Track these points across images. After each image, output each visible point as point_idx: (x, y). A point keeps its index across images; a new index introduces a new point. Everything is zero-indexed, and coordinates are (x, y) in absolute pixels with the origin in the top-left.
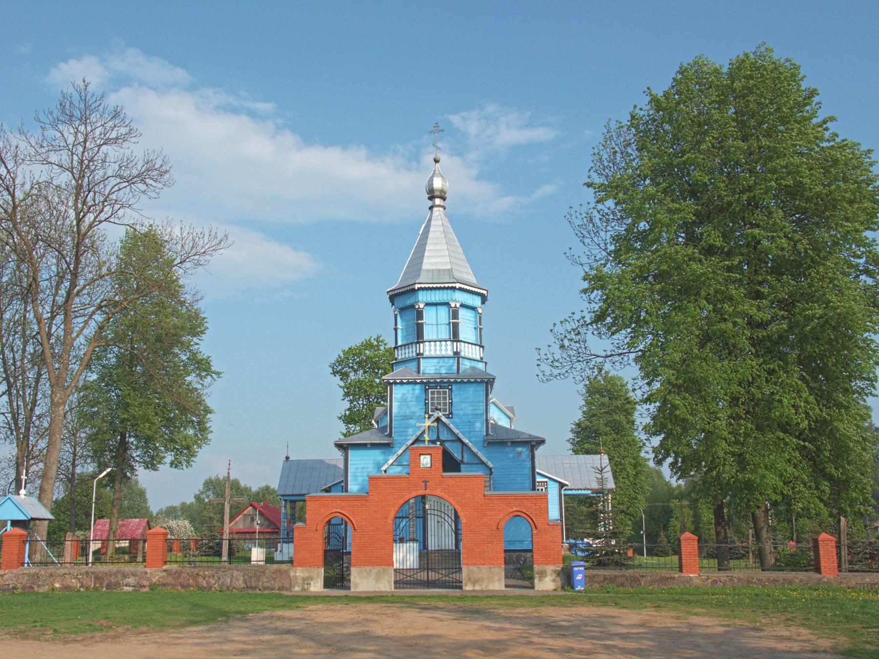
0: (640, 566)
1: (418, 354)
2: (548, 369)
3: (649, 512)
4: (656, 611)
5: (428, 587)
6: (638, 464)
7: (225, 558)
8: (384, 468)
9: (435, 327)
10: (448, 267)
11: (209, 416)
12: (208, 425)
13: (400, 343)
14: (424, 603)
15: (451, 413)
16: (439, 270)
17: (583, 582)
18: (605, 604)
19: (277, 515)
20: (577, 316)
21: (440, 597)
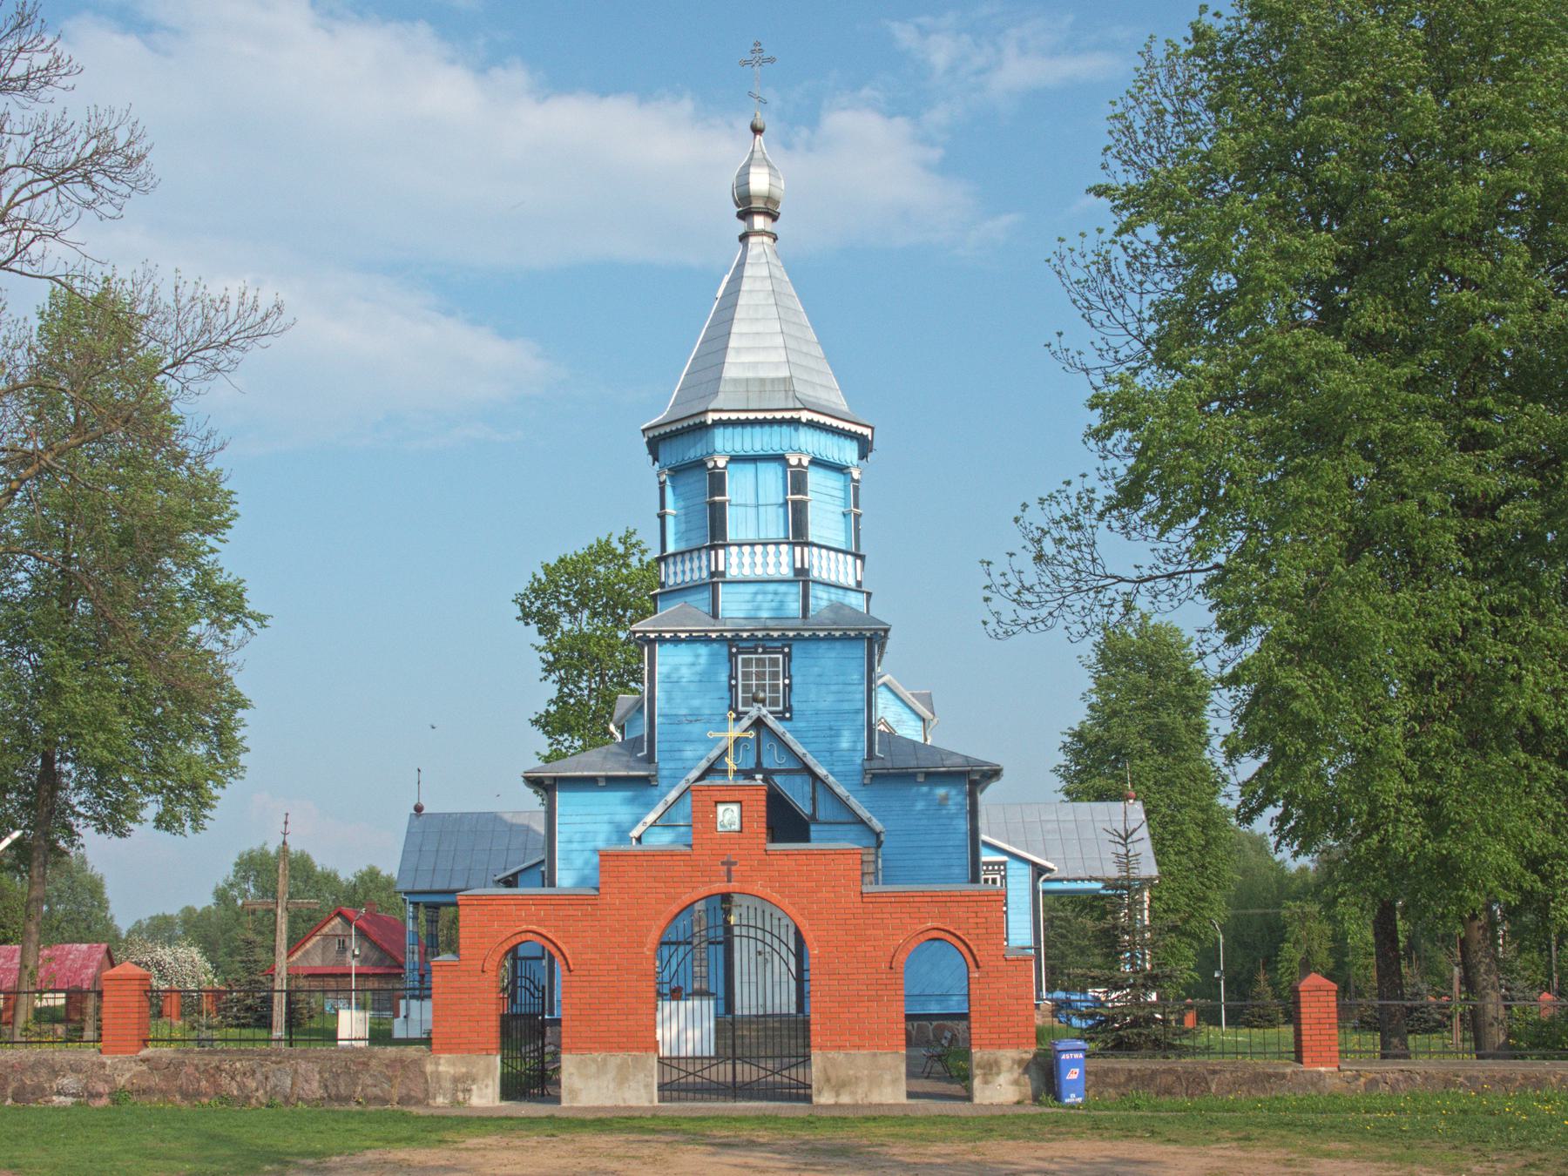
0: (1208, 1050)
1: (712, 575)
2: (1008, 610)
4: (1241, 1148)
5: (735, 1098)
6: (1210, 822)
7: (279, 1032)
8: (635, 833)
9: (752, 511)
10: (784, 373)
11: (240, 713)
12: (238, 735)
13: (671, 549)
14: (723, 1133)
15: (789, 709)
16: (762, 381)
17: (1082, 1085)
18: (1127, 1133)
19: (398, 936)
21: (762, 1120)
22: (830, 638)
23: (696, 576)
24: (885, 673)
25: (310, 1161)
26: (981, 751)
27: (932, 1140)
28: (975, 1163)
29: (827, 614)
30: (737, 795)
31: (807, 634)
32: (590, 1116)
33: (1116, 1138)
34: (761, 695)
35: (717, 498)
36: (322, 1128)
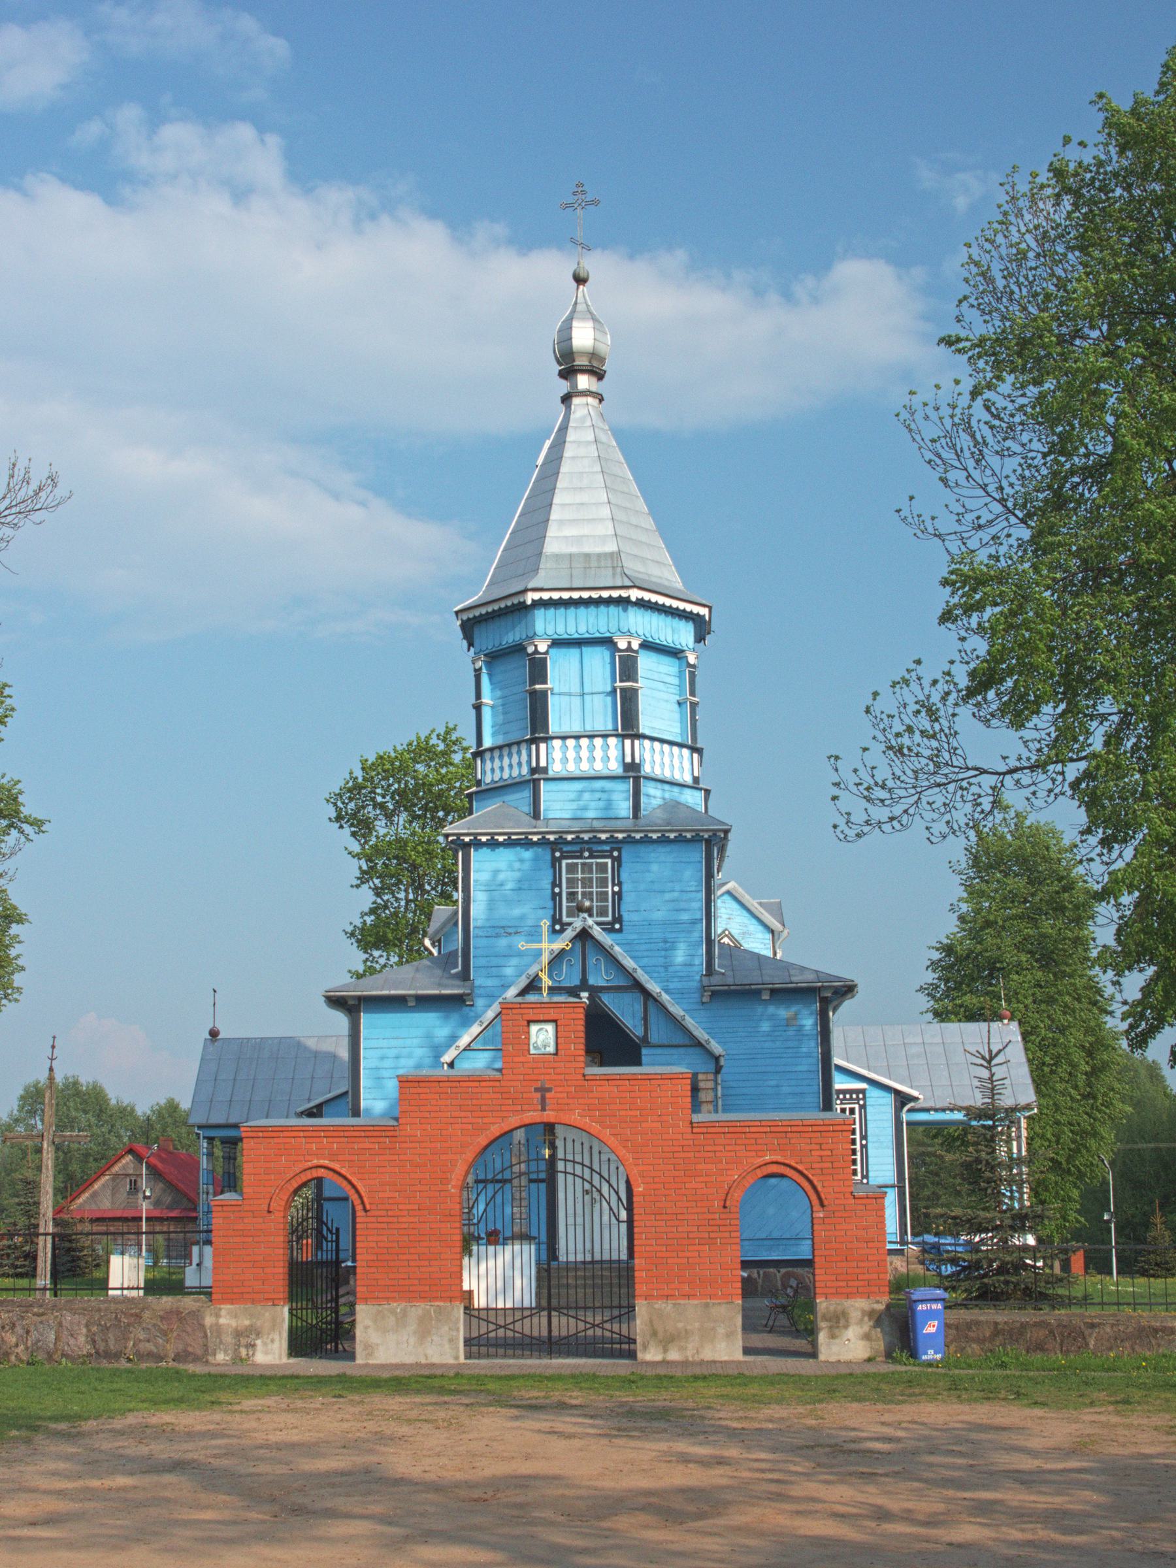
0: (1085, 1300)
1: (533, 771)
2: (852, 803)
3: (1125, 1167)
4: (1118, 1413)
5: (551, 1354)
6: (1097, 1044)
7: (43, 1280)
8: (447, 1058)
9: (576, 701)
10: (611, 547)
11: (15, 929)
12: (13, 952)
13: (488, 742)
14: (534, 1394)
15: (618, 919)
16: (587, 556)
17: (941, 1341)
18: (989, 1394)
19: (182, 1172)
20: (929, 672)
21: (577, 1379)
22: (664, 841)
23: (515, 773)
24: (728, 879)
25: (63, 1426)
26: (837, 968)
27: (768, 1402)
28: (810, 1428)
29: (659, 814)
30: (552, 1014)
31: (638, 836)
32: (386, 1375)
33: (976, 1400)
34: (587, 904)
35: (537, 686)
36: (83, 1388)
